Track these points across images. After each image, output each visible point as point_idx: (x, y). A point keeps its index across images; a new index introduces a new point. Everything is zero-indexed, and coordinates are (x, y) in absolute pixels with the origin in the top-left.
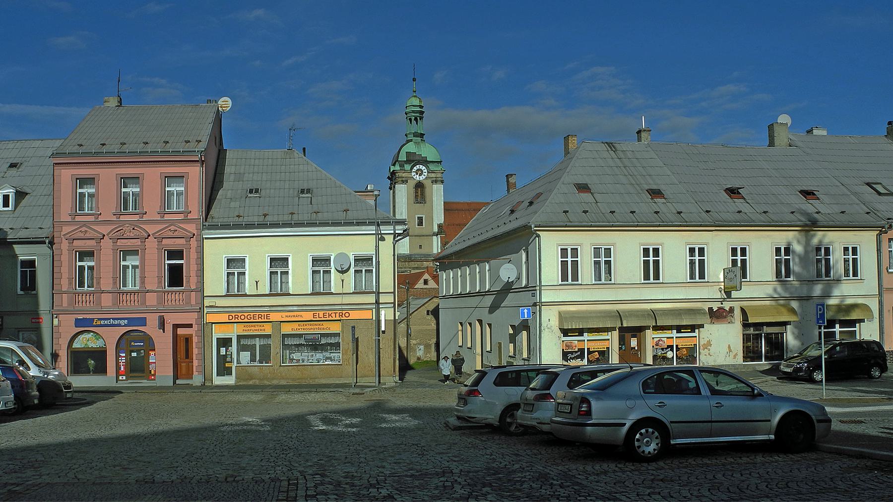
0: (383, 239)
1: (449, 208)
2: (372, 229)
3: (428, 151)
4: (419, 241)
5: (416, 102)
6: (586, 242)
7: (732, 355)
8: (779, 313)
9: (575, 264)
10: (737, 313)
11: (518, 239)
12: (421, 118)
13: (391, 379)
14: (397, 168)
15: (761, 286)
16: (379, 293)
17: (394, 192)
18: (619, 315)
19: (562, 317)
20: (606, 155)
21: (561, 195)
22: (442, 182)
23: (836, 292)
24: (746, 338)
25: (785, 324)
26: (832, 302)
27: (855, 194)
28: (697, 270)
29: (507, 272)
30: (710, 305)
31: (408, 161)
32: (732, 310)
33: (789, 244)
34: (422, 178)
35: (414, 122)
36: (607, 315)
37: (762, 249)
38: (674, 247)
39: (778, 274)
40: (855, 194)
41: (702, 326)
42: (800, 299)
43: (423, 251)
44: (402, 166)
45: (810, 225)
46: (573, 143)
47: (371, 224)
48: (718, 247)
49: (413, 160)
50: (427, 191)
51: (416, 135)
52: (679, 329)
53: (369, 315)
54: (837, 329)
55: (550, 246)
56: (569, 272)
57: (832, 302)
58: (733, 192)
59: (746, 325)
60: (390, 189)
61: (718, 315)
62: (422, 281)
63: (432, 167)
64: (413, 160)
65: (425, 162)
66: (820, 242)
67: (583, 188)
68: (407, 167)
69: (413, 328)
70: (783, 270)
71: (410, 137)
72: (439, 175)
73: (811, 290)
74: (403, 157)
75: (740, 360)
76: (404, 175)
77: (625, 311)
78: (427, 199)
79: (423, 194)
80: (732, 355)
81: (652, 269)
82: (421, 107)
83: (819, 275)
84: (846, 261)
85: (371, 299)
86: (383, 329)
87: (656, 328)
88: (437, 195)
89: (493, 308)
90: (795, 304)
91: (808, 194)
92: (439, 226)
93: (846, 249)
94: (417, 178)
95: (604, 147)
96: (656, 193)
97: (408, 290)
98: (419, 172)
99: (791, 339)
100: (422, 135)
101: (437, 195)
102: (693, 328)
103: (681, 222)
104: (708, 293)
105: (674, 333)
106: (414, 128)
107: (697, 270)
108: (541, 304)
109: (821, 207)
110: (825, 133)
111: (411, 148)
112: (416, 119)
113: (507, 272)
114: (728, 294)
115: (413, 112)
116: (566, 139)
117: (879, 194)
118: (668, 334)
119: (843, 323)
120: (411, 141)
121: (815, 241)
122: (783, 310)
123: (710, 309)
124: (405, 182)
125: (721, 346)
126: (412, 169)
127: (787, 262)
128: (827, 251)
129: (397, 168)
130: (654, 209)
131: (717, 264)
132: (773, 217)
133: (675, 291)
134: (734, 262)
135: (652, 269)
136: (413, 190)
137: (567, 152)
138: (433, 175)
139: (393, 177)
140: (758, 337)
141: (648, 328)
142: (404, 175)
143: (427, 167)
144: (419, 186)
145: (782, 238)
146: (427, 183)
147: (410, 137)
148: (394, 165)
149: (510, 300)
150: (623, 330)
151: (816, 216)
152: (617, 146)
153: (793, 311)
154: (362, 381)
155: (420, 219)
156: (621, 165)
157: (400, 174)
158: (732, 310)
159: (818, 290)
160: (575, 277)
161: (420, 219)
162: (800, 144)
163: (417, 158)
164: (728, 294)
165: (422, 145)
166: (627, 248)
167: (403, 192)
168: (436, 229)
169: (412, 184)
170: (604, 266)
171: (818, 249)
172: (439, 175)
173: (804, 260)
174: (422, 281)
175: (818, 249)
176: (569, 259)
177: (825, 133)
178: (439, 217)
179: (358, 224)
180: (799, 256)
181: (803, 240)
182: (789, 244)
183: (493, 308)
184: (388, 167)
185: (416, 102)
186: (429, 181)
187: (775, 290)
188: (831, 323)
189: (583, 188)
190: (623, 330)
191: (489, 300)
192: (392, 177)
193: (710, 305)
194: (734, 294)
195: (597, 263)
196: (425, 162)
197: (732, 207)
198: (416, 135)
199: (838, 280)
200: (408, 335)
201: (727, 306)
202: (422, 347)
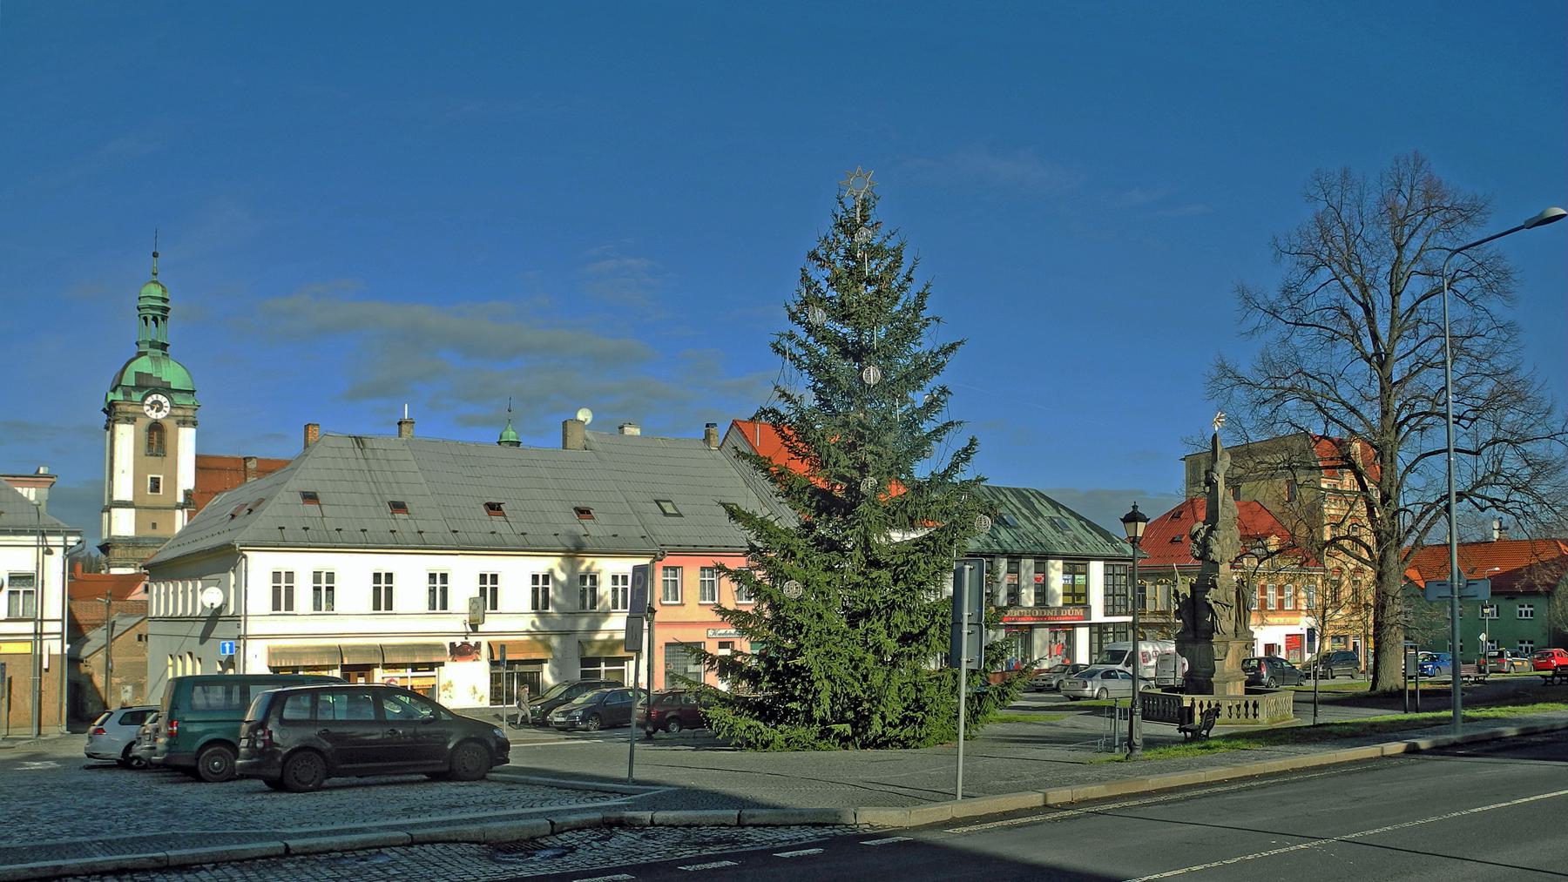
0: (50, 552)
1: (203, 465)
2: (32, 539)
3: (173, 373)
4: (151, 516)
5: (156, 291)
6: (303, 565)
7: (477, 696)
8: (533, 651)
9: (290, 590)
10: (484, 649)
11: (221, 560)
12: (164, 319)
13: (56, 727)
14: (119, 396)
15: (514, 617)
16: (42, 620)
17: (112, 436)
18: (340, 651)
19: (273, 654)
20: (349, 453)
21: (283, 505)
22: (194, 424)
23: (604, 626)
24: (495, 679)
25: (541, 662)
26: (600, 637)
27: (638, 513)
28: (438, 596)
29: (211, 597)
30: (452, 640)
31: (138, 387)
32: (478, 645)
33: (551, 571)
34: (161, 415)
35: (151, 323)
36: (328, 651)
37: (517, 574)
38: (411, 572)
39: (535, 606)
40: (638, 513)
41: (442, 664)
42: (562, 633)
43: (158, 533)
44: (127, 394)
45: (575, 551)
46: (314, 434)
47: (32, 533)
48: (464, 572)
49: (147, 385)
50: (169, 436)
51: (153, 345)
52: (415, 667)
53: (26, 648)
54: (603, 667)
55: (260, 566)
56: (282, 599)
57: (600, 637)
58: (493, 508)
59: (494, 663)
60: (107, 428)
61: (462, 652)
62: (141, 588)
63: (178, 399)
64: (147, 385)
65: (167, 390)
66: (588, 569)
67: (310, 497)
68: (137, 397)
69: (117, 660)
70: (540, 601)
71: (145, 348)
72: (190, 413)
73: (575, 623)
74: (129, 379)
75: (486, 703)
76: (130, 409)
77: (346, 647)
78: (169, 449)
79: (161, 441)
80: (477, 696)
81: (383, 597)
82: (165, 300)
83: (584, 606)
84: (615, 591)
85: (29, 627)
86: (45, 665)
87: (386, 666)
88: (186, 442)
89: (204, 638)
90: (555, 641)
91: (583, 512)
92: (187, 494)
93: (615, 578)
94: (153, 415)
95: (350, 443)
96: (398, 507)
97: (109, 605)
98: (158, 406)
99: (547, 676)
100: (164, 346)
101: (186, 442)
102: (431, 666)
103: (422, 544)
104: (452, 624)
105: (409, 672)
106: (153, 333)
107: (438, 596)
108: (246, 637)
109: (593, 529)
110: (637, 432)
111: (144, 365)
112: (155, 319)
113: (211, 597)
114: (474, 627)
115: (151, 307)
116: (306, 427)
117: (665, 514)
118: (402, 672)
119: (609, 661)
120: (145, 354)
121: (583, 568)
122: (539, 646)
123: (452, 645)
124: (130, 420)
125: (464, 688)
126: (144, 399)
127: (546, 591)
128: (593, 578)
129: (119, 396)
130: (396, 525)
131: (463, 589)
132: (531, 540)
133: (411, 620)
134: (483, 591)
135: (383, 597)
136: (144, 435)
137: (307, 445)
138: (180, 412)
139: (112, 413)
140: (510, 677)
141: (377, 666)
142: (130, 409)
143: (170, 399)
144: (156, 427)
145: (542, 564)
146: (170, 425)
147: (145, 348)
148: (114, 390)
149: (220, 629)
150: (344, 668)
151: (584, 539)
152: (367, 442)
153: (548, 648)
154: (15, 733)
155: (156, 482)
156: (365, 467)
157: (124, 408)
158: (478, 645)
159: (583, 624)
160: (290, 606)
161: (156, 482)
162: (597, 446)
163: (154, 383)
164: (474, 627)
165: (164, 363)
166: (354, 572)
167: (126, 437)
168: (180, 499)
169: (143, 424)
170: (324, 592)
171: (583, 578)
172: (190, 413)
173: (566, 588)
174: (141, 588)
175: (583, 578)
176: (283, 585)
177: (637, 432)
178: (186, 478)
179: (15, 533)
180: (562, 585)
181: (568, 568)
182: (551, 571)
183: (204, 638)
184: (103, 393)
185: (156, 291)
186: (173, 421)
187: (533, 624)
188: (595, 661)
189: (310, 497)
190: (344, 668)
191: (199, 628)
192: (111, 410)
193: (452, 640)
194: (481, 628)
195: (317, 590)
196: (167, 390)
197: (493, 526)
198: (153, 345)
199: (607, 614)
200: (109, 671)
201: (472, 640)
202: (129, 688)
